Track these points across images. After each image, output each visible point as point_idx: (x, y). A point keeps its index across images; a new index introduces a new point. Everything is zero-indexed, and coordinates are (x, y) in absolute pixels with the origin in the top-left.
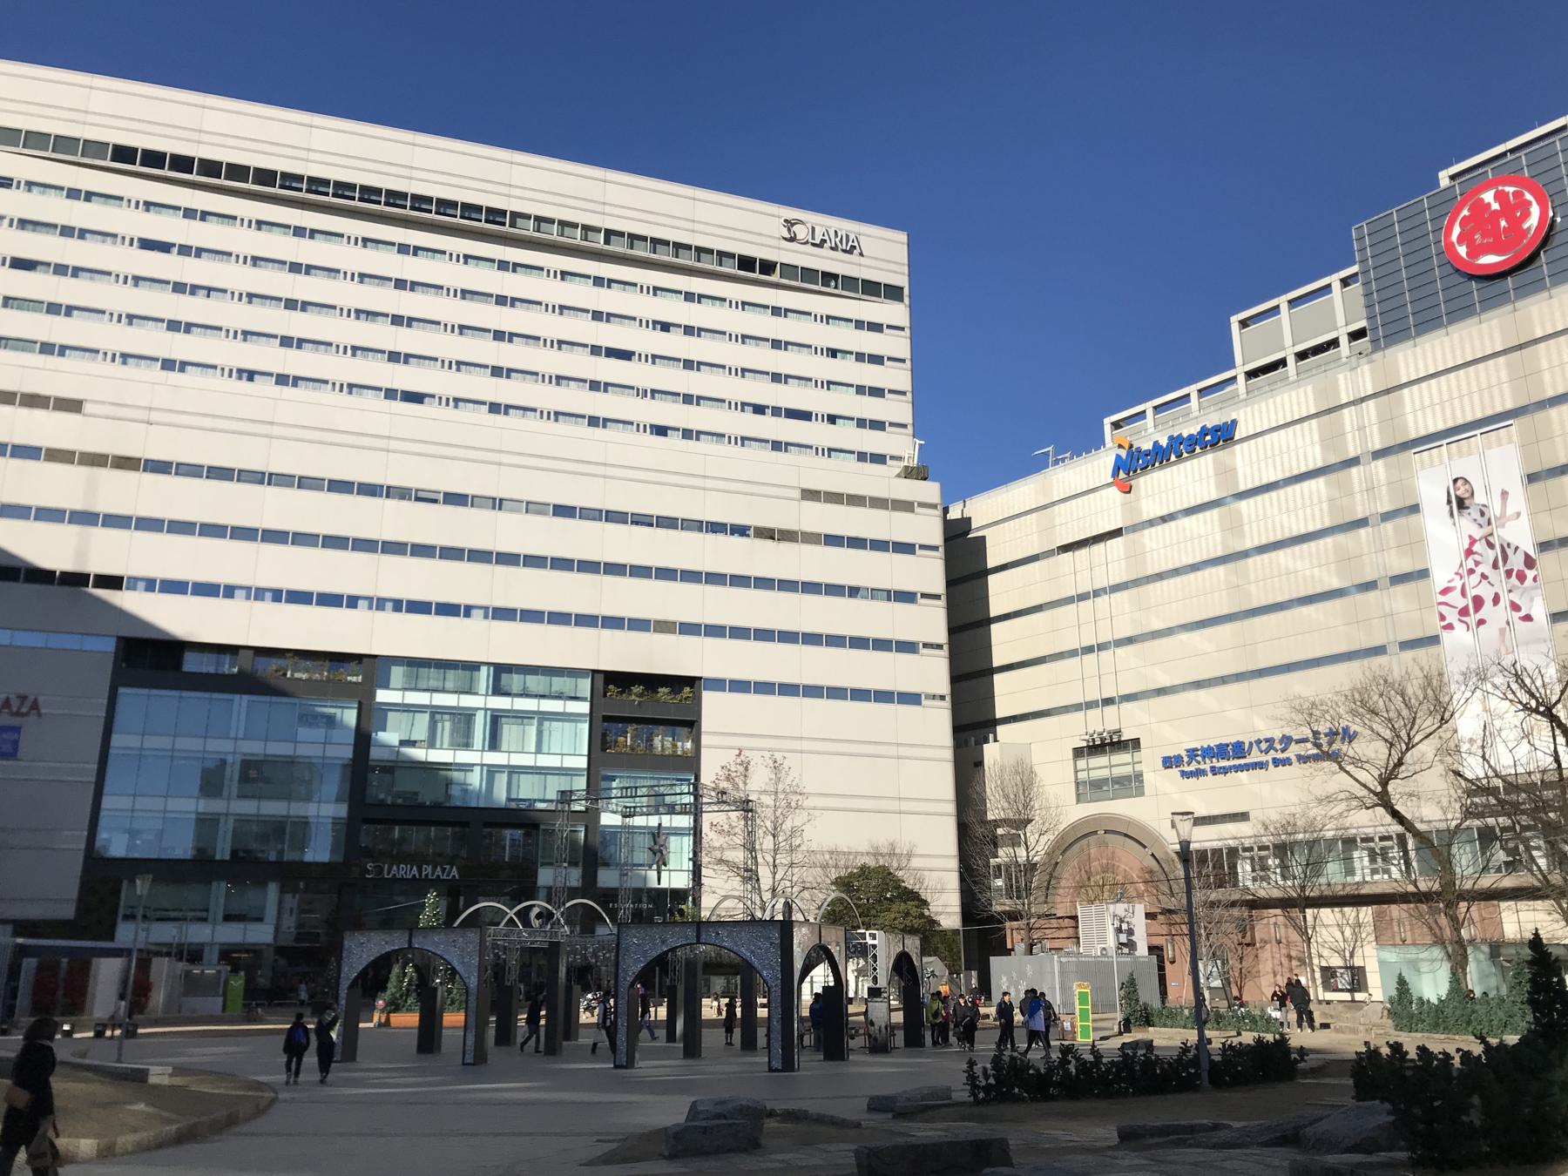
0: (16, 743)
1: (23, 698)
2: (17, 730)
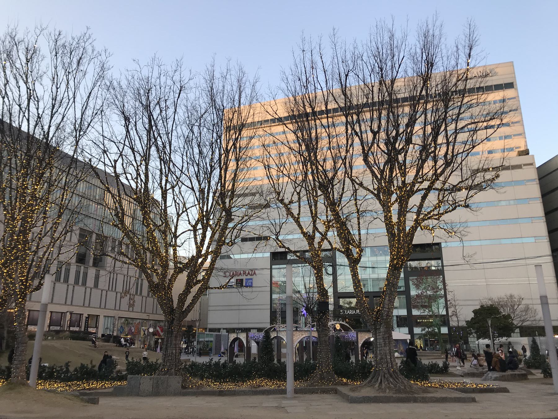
0: (252, 283)
1: (252, 270)
2: (252, 279)
